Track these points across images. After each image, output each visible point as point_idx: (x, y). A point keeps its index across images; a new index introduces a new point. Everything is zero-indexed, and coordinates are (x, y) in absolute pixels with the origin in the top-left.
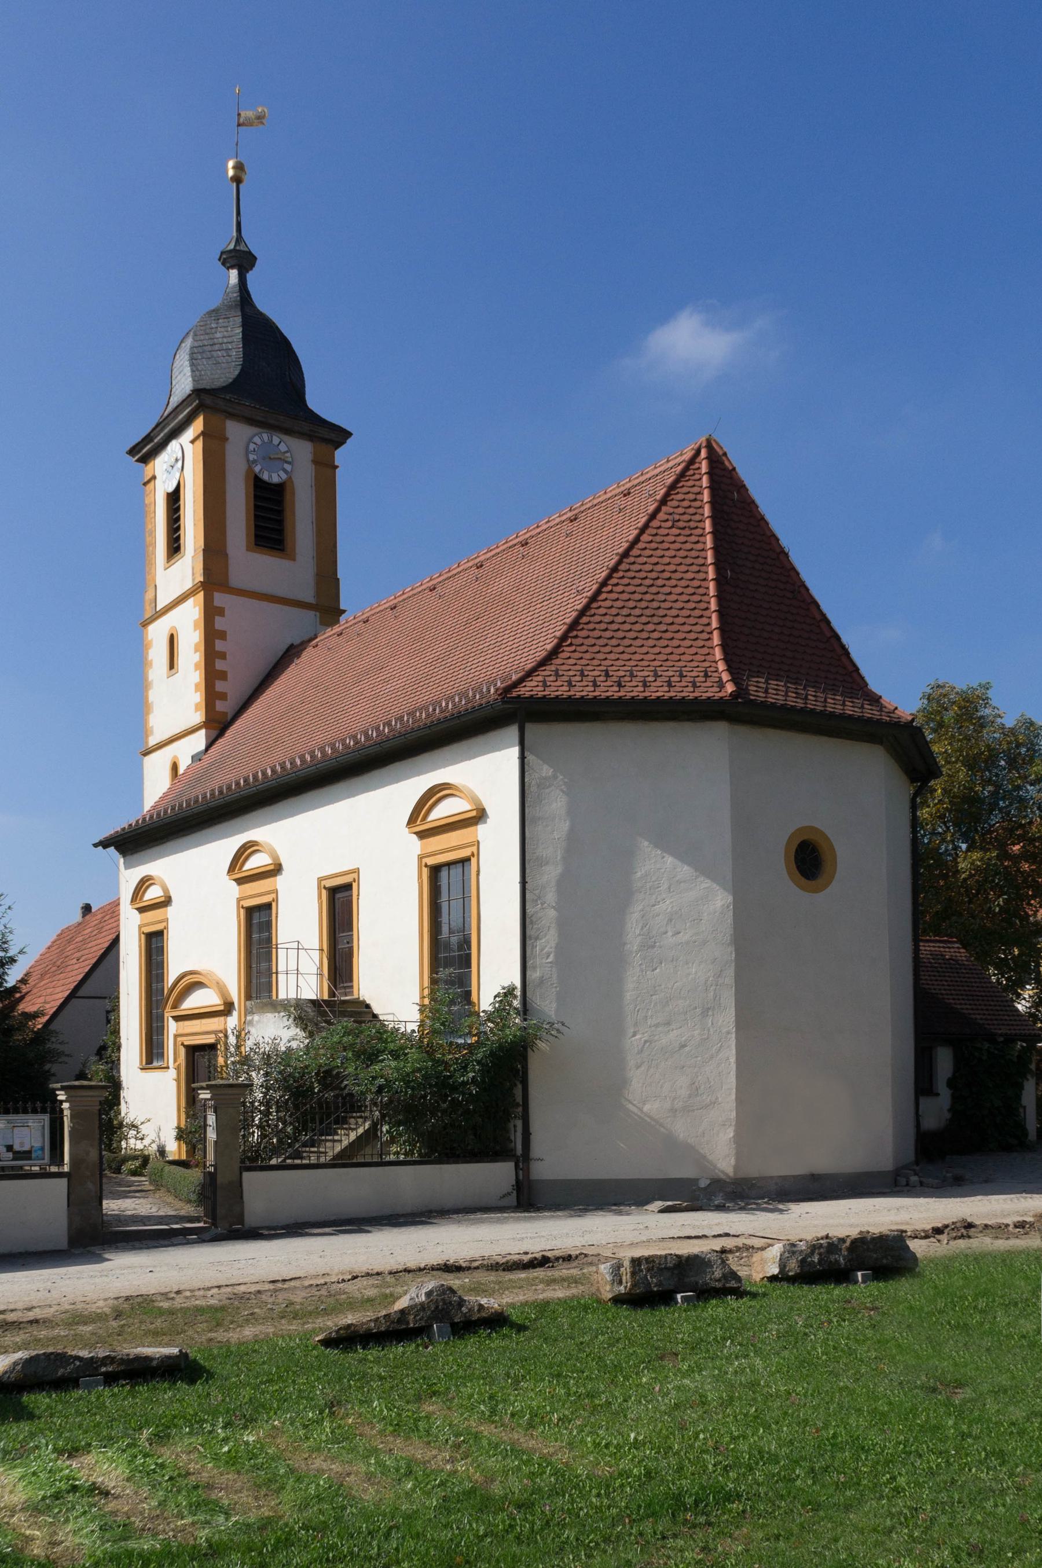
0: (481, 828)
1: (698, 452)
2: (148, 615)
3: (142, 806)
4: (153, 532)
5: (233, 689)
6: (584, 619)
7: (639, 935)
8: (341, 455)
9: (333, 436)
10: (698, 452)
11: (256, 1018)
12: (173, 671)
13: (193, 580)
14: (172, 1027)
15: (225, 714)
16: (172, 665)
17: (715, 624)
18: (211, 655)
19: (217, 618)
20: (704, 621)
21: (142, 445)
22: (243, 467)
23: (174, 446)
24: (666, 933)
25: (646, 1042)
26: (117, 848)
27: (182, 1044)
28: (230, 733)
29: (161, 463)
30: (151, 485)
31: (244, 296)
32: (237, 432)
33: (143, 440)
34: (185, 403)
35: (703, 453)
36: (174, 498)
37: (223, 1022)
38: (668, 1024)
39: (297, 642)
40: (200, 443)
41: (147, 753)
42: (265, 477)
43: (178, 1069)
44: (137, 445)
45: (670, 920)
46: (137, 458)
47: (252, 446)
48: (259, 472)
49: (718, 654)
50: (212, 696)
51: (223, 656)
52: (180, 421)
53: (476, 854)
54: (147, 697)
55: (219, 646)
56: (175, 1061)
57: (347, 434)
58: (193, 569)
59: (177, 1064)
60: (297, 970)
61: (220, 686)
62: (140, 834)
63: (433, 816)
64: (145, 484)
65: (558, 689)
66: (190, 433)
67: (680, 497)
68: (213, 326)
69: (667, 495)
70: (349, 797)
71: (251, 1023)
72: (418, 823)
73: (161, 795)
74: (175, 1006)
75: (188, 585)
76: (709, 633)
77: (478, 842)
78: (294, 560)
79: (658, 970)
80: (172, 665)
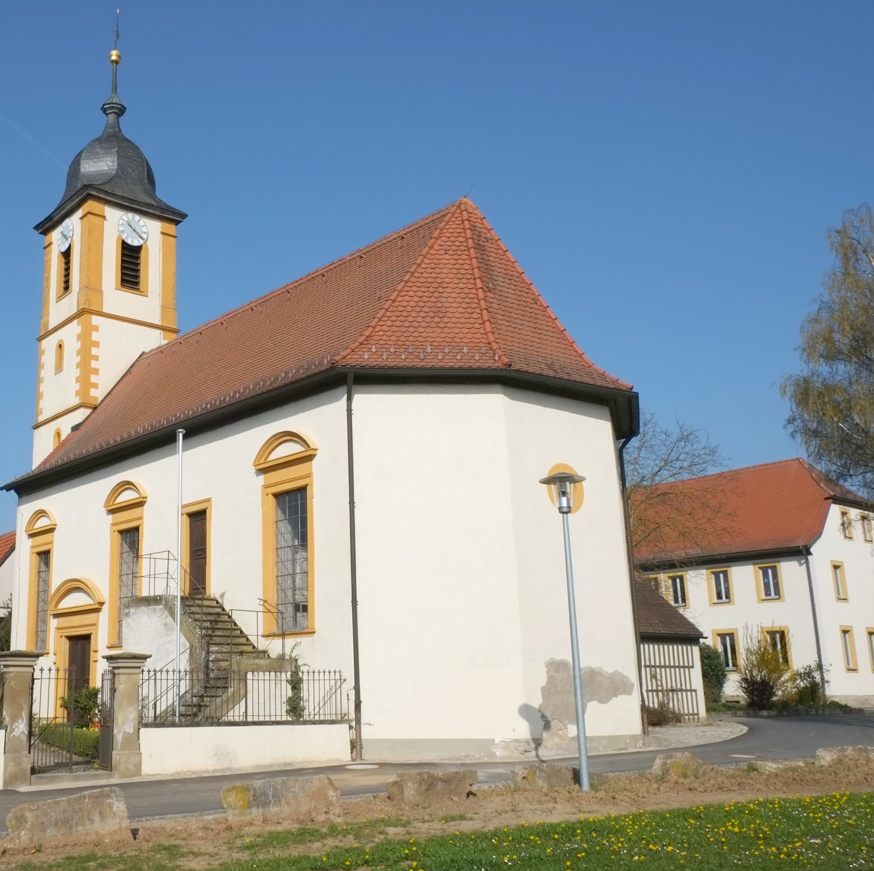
2: (43, 333)
3: (31, 465)
4: (48, 279)
11: (132, 610)
13: (78, 308)
15: (97, 398)
19: (94, 333)
21: (44, 223)
26: (16, 491)
29: (55, 235)
30: (47, 249)
33: (46, 219)
34: (78, 193)
41: (37, 427)
44: (41, 223)
46: (40, 231)
48: (126, 238)
52: (73, 205)
54: (38, 389)
57: (184, 216)
58: (78, 300)
60: (168, 573)
62: (37, 479)
64: (45, 248)
70: (160, 459)
71: (127, 615)
73: (49, 454)
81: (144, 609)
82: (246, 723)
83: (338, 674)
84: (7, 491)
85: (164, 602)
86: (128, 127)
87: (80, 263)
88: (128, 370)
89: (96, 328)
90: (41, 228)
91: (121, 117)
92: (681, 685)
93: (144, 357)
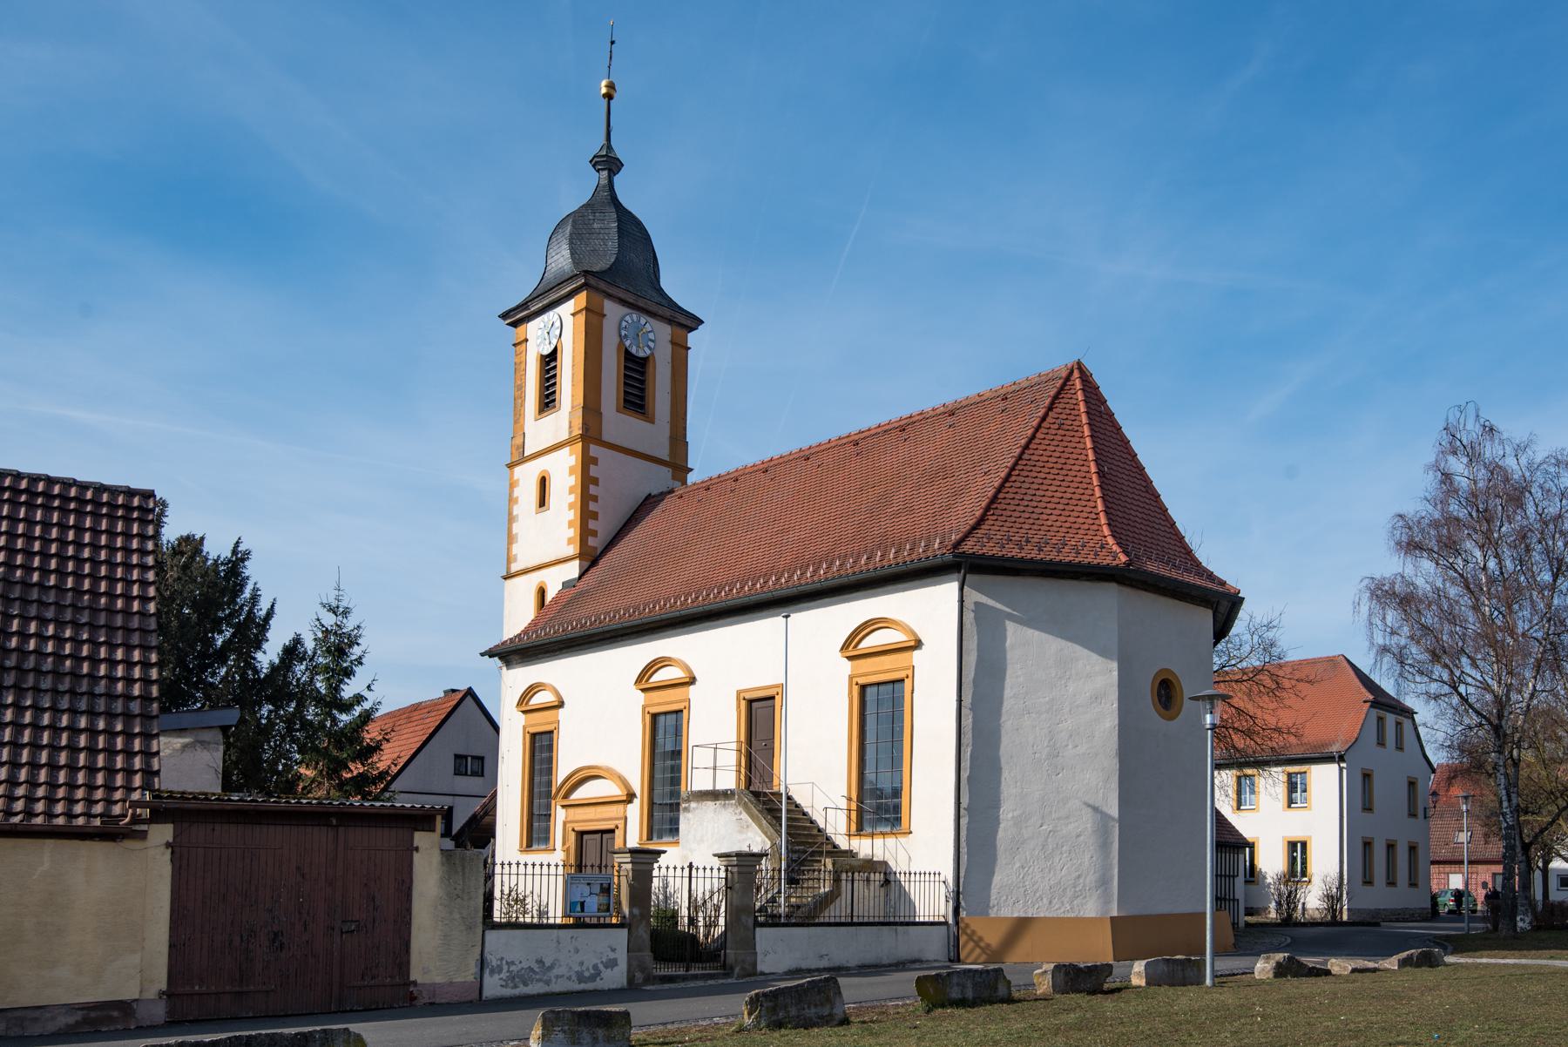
0: (916, 653)
1: (1071, 373)
3: (499, 624)
5: (604, 527)
6: (1001, 495)
7: (1047, 746)
8: (692, 338)
9: (689, 323)
10: (1071, 373)
11: (693, 805)
12: (543, 508)
13: (570, 433)
14: (560, 815)
15: (596, 548)
16: (542, 502)
17: (1100, 507)
18: (586, 498)
20: (1092, 504)
22: (616, 340)
23: (551, 316)
24: (1067, 745)
25: (1050, 831)
26: (500, 658)
27: (573, 830)
28: (603, 562)
29: (534, 329)
31: (608, 199)
32: (612, 309)
35: (1076, 374)
36: (550, 361)
37: (622, 810)
38: (1068, 817)
39: (654, 492)
40: (582, 318)
42: (633, 350)
43: (567, 851)
45: (1071, 736)
47: (624, 324)
49: (1106, 531)
50: (585, 533)
51: (595, 499)
53: (910, 676)
55: (593, 490)
56: (564, 844)
58: (570, 422)
59: (566, 847)
61: (592, 525)
63: (862, 645)
65: (991, 549)
66: (568, 308)
67: (1061, 406)
68: (590, 217)
69: (1052, 403)
72: (850, 649)
74: (566, 796)
75: (564, 436)
76: (1096, 514)
77: (913, 667)
78: (653, 423)
79: (1060, 775)
80: (542, 502)
81: (710, 804)
82: (852, 924)
83: (937, 875)
84: (490, 657)
85: (736, 797)
86: (629, 192)
87: (573, 374)
88: (632, 516)
89: (595, 461)
90: (509, 318)
91: (617, 176)
92: (1225, 895)
93: (652, 500)
